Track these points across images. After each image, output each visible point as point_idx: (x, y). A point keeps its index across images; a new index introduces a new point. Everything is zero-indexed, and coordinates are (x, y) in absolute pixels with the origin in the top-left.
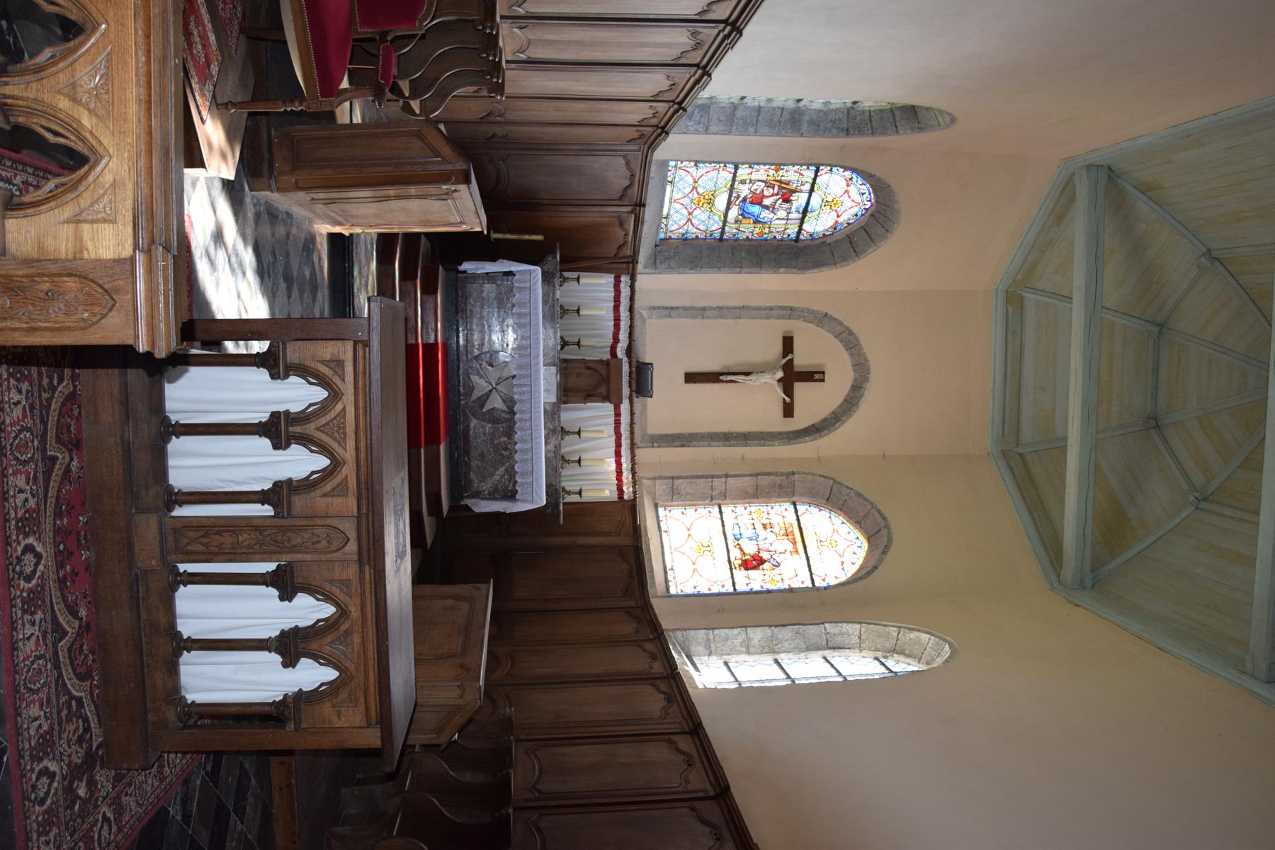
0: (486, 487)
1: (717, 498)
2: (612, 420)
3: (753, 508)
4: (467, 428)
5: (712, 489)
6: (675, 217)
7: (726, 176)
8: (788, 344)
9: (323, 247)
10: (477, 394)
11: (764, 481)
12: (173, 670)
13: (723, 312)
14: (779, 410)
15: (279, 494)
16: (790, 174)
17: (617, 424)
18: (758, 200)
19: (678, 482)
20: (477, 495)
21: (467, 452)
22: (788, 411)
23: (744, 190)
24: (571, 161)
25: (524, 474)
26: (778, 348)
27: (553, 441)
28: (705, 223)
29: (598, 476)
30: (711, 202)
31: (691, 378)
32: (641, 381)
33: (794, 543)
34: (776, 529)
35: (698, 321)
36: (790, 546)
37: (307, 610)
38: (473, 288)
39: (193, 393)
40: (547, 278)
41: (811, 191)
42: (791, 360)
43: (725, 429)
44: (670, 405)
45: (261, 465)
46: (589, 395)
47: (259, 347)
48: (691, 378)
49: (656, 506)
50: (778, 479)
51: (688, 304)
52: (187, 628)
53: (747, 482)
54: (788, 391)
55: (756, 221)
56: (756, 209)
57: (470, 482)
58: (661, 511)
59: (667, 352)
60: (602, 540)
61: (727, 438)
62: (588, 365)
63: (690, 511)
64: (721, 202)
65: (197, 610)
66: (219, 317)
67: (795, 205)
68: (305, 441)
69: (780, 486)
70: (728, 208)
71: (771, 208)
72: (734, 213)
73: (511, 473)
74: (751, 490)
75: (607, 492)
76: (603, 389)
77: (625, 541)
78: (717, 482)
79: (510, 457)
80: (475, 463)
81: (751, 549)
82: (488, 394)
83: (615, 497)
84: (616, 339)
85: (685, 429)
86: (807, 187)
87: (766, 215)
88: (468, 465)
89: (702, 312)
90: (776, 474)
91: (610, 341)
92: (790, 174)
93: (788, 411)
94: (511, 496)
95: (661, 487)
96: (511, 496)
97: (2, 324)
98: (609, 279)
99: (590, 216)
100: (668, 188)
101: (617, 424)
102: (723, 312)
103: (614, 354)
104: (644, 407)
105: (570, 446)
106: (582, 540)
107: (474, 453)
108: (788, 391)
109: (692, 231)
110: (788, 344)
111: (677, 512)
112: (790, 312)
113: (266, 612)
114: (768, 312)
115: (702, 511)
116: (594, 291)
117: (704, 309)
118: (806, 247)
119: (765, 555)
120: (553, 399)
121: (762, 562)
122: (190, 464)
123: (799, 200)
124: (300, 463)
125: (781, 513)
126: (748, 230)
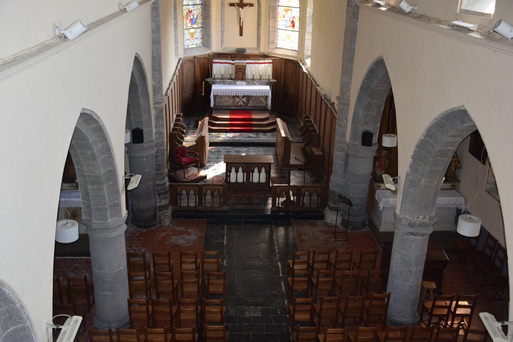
0: (265, 102)
1: (276, 30)
2: (251, 65)
3: (279, 19)
4: (250, 106)
5: (273, 31)
6: (196, 42)
7: (186, 32)
8: (232, 5)
9: (211, 148)
10: (242, 104)
11: (271, 16)
12: (262, 183)
13: (222, 26)
14: (251, 8)
15: (243, 172)
16: (185, 13)
17: (252, 63)
18: (191, 20)
19: (270, 41)
20: (267, 105)
21: (256, 107)
22: (251, 5)
23: (189, 25)
24: (185, 77)
25: (262, 93)
26: (233, 7)
27: (255, 83)
28: (198, 34)
29: (264, 69)
30: (192, 34)
31: (241, 34)
32: (240, 54)
33: (289, 10)
34: (285, 14)
35: (225, 32)
36: (289, 11)
37: (256, 170)
38: (217, 104)
39: (233, 179)
40: (214, 83)
41: (188, 5)
42: (237, 4)
43: (256, 24)
44: (247, 42)
45: (240, 174)
46: (244, 73)
47: (218, 301)
48: (241, 34)
49: (276, 48)
50: (271, 11)
51: (220, 36)
52: (258, 181)
53: (271, 21)
54: (246, 5)
55: (197, 18)
56: (194, 20)
57: (263, 106)
58: (278, 46)
59: (233, 43)
60: (283, 68)
61: (259, 25)
62: (236, 73)
63: (279, 38)
64: (192, 31)
65: (255, 180)
66: (225, 171)
67: (193, 9)
68: (238, 169)
69: (273, 10)
70: (193, 28)
71: (193, 15)
72: (195, 26)
73: (262, 96)
74: (274, 19)
75: (269, 68)
76: (242, 70)
77: (284, 61)
78: (271, 30)
79: (258, 97)
80: (259, 105)
81: (289, 24)
82: (243, 101)
83: (272, 64)
84: (230, 63)
85: (256, 36)
86: (187, 7)
87: (195, 17)
88: (259, 107)
89: (222, 35)
90: (269, 12)
91: (230, 65)
92: (185, 13)
93: (251, 5)
94: (267, 97)
95: (271, 46)
96: (267, 97)
97: (185, 333)
98: (214, 65)
99: (198, 69)
100: (190, 47)
101: (252, 63)
102: (222, 26)
103: (234, 64)
104: (250, 48)
105: (257, 77)
106: (283, 73)
107: (257, 105)
108: (246, 5)
109: (201, 36)
110: (232, 5)
111: (279, 42)
112: (222, 5)
113: (256, 174)
114: (222, 11)
115: (279, 34)
116: (219, 68)
117: (222, 31)
118: (204, 2)
119: (291, 20)
120: (244, 83)
121: (293, 21)
122: (240, 180)
123: (191, 8)
124: (240, 170)
125: (281, 11)
126: (199, 21)
